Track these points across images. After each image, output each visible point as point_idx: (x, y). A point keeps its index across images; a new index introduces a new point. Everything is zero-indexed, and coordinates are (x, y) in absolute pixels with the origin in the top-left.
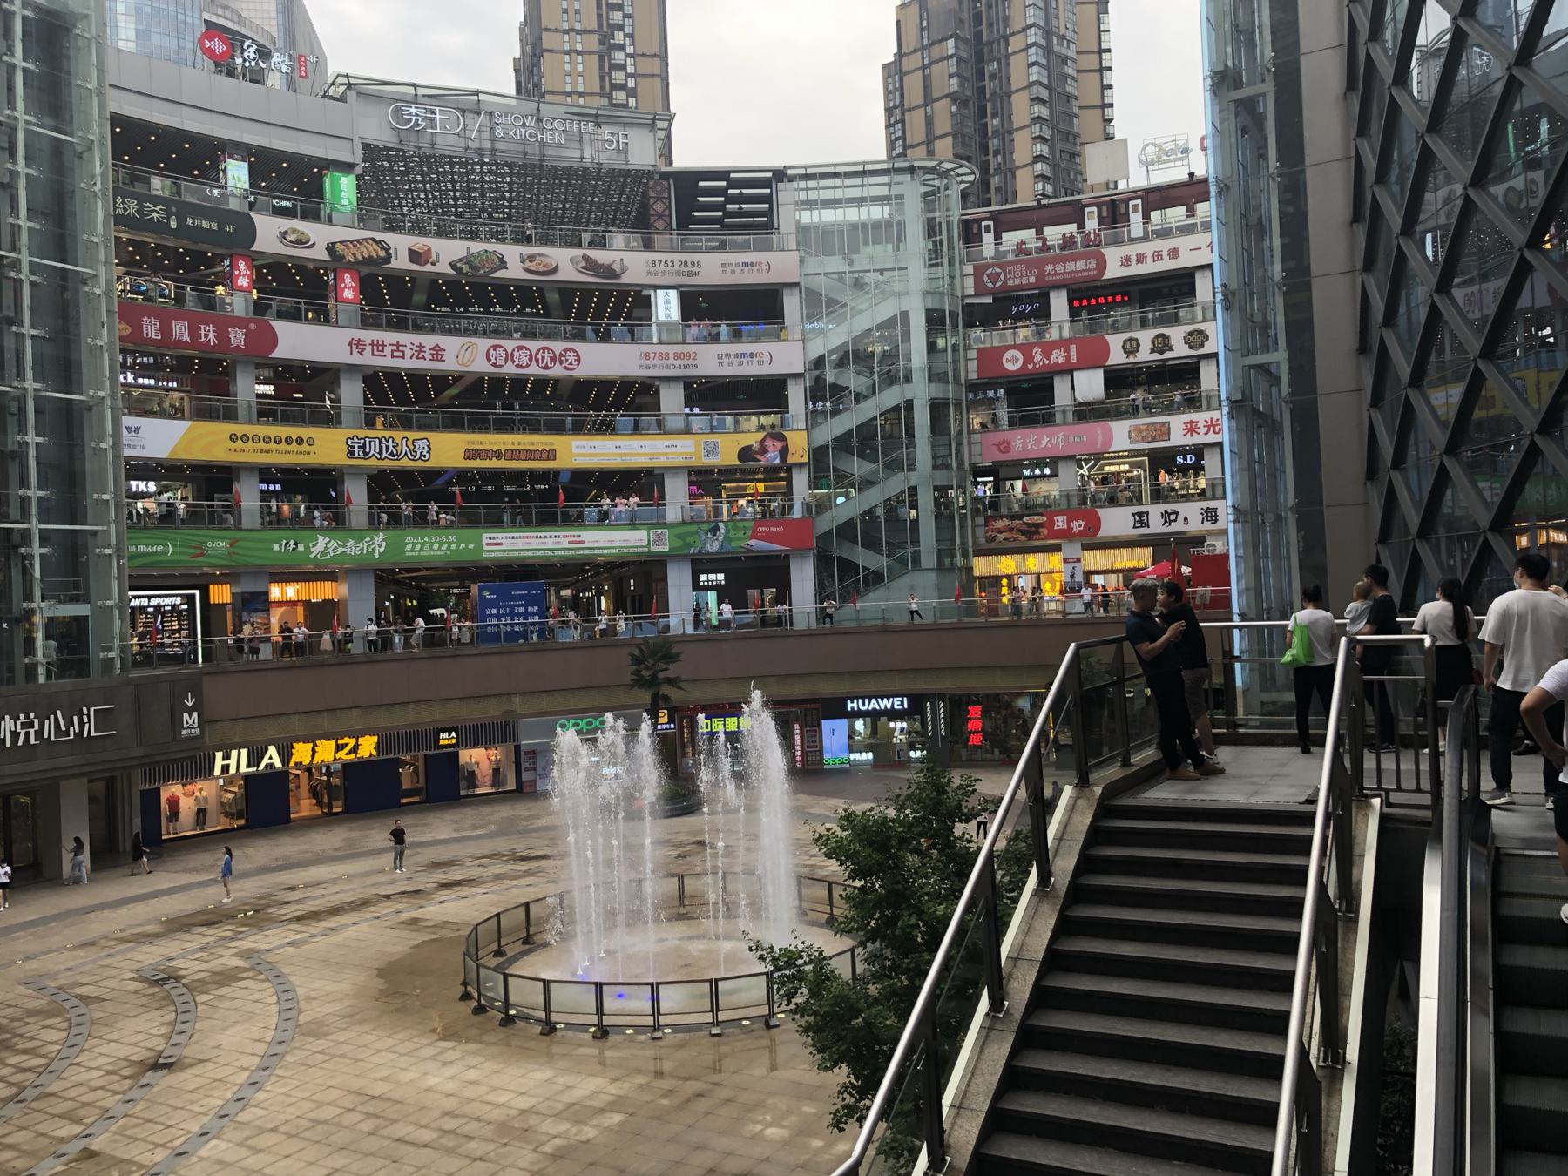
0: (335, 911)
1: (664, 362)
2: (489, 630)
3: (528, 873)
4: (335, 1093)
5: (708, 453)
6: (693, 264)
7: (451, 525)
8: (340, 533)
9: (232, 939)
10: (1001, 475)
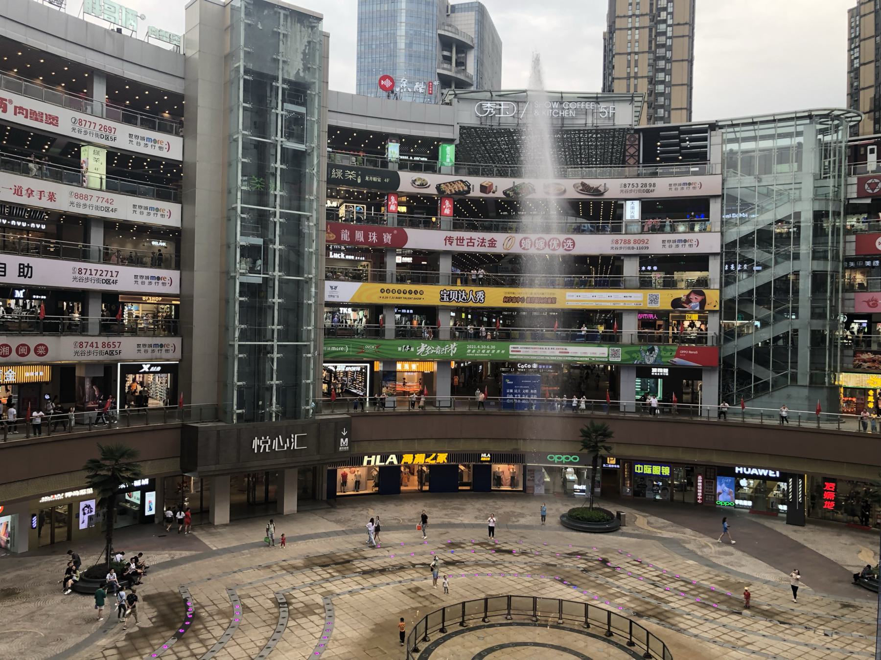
1: (627, 245)
2: (508, 401)
3: (494, 564)
6: (650, 185)
8: (434, 342)
9: (327, 580)
10: (873, 319)
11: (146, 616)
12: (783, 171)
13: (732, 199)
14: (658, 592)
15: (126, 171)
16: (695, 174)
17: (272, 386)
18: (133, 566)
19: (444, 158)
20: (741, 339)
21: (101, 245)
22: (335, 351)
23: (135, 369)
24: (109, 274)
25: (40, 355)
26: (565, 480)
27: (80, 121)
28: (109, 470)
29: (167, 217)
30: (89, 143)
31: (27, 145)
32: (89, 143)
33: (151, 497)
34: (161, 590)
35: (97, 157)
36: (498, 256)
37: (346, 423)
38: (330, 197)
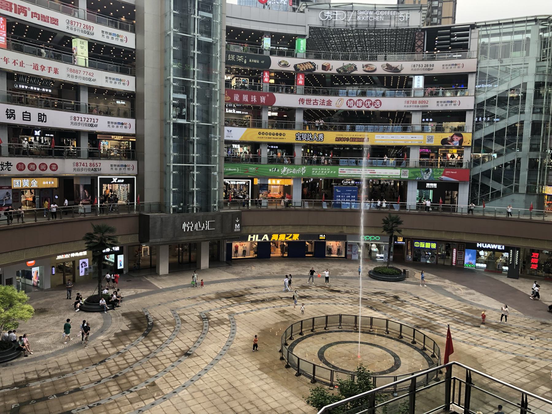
0: (263, 301)
1: (415, 104)
2: (337, 203)
3: (330, 298)
4: (225, 381)
5: (429, 140)
6: (430, 65)
7: (328, 164)
9: (230, 306)
11: (124, 325)
12: (517, 56)
13: (483, 74)
14: (430, 315)
15: (101, 54)
16: (459, 58)
17: (193, 191)
18: (115, 296)
19: (299, 47)
20: (484, 164)
21: (87, 102)
22: (231, 171)
23: (109, 181)
24: (93, 120)
25: (53, 170)
26: (371, 252)
27: (72, 22)
28: (98, 240)
29: (126, 85)
30: (77, 37)
31: (38, 38)
32: (77, 37)
33: (121, 258)
34: (132, 310)
35: (82, 45)
36: (332, 112)
37: (239, 215)
38: (227, 73)
